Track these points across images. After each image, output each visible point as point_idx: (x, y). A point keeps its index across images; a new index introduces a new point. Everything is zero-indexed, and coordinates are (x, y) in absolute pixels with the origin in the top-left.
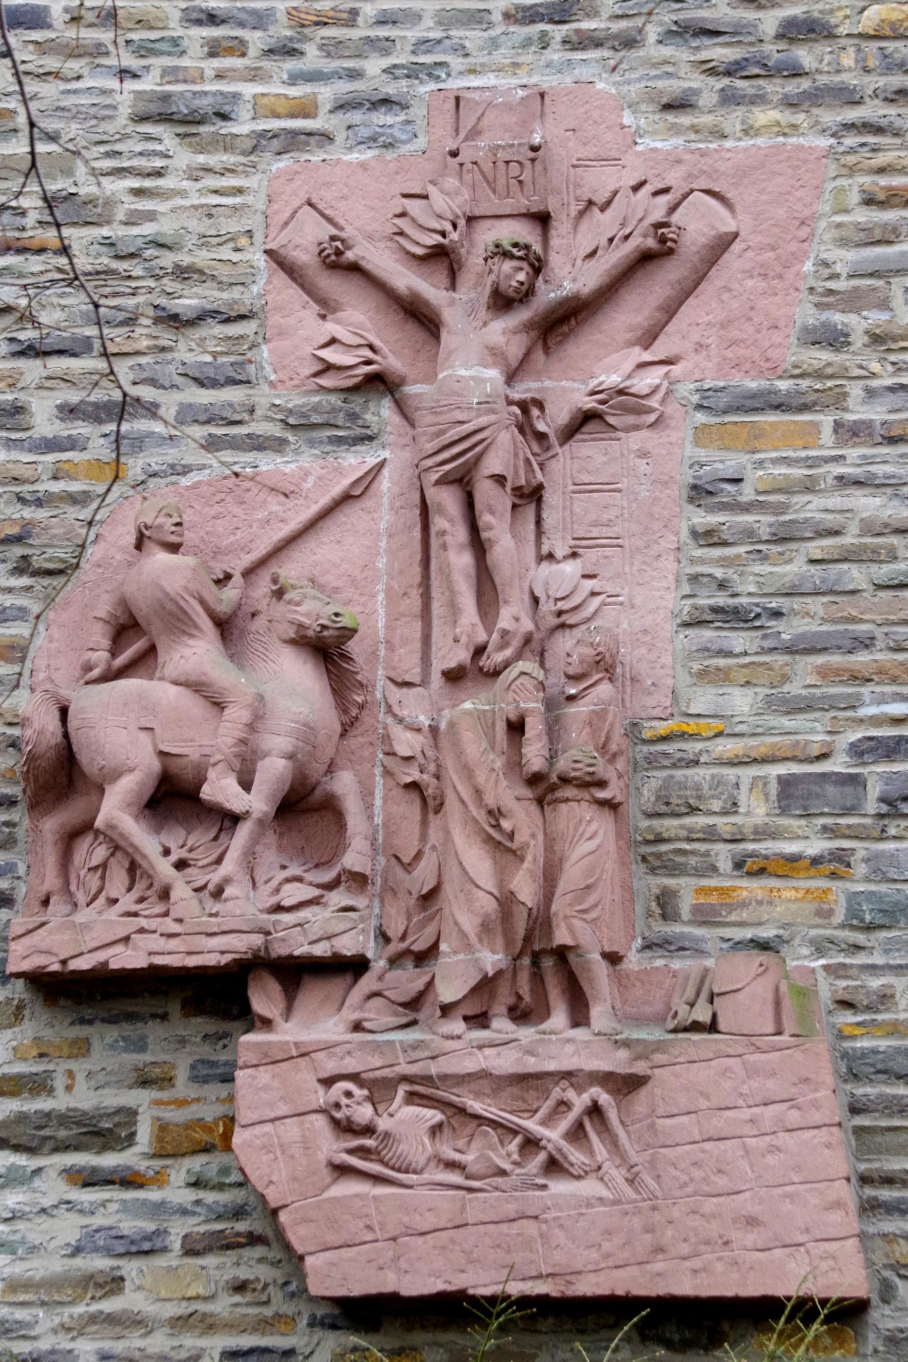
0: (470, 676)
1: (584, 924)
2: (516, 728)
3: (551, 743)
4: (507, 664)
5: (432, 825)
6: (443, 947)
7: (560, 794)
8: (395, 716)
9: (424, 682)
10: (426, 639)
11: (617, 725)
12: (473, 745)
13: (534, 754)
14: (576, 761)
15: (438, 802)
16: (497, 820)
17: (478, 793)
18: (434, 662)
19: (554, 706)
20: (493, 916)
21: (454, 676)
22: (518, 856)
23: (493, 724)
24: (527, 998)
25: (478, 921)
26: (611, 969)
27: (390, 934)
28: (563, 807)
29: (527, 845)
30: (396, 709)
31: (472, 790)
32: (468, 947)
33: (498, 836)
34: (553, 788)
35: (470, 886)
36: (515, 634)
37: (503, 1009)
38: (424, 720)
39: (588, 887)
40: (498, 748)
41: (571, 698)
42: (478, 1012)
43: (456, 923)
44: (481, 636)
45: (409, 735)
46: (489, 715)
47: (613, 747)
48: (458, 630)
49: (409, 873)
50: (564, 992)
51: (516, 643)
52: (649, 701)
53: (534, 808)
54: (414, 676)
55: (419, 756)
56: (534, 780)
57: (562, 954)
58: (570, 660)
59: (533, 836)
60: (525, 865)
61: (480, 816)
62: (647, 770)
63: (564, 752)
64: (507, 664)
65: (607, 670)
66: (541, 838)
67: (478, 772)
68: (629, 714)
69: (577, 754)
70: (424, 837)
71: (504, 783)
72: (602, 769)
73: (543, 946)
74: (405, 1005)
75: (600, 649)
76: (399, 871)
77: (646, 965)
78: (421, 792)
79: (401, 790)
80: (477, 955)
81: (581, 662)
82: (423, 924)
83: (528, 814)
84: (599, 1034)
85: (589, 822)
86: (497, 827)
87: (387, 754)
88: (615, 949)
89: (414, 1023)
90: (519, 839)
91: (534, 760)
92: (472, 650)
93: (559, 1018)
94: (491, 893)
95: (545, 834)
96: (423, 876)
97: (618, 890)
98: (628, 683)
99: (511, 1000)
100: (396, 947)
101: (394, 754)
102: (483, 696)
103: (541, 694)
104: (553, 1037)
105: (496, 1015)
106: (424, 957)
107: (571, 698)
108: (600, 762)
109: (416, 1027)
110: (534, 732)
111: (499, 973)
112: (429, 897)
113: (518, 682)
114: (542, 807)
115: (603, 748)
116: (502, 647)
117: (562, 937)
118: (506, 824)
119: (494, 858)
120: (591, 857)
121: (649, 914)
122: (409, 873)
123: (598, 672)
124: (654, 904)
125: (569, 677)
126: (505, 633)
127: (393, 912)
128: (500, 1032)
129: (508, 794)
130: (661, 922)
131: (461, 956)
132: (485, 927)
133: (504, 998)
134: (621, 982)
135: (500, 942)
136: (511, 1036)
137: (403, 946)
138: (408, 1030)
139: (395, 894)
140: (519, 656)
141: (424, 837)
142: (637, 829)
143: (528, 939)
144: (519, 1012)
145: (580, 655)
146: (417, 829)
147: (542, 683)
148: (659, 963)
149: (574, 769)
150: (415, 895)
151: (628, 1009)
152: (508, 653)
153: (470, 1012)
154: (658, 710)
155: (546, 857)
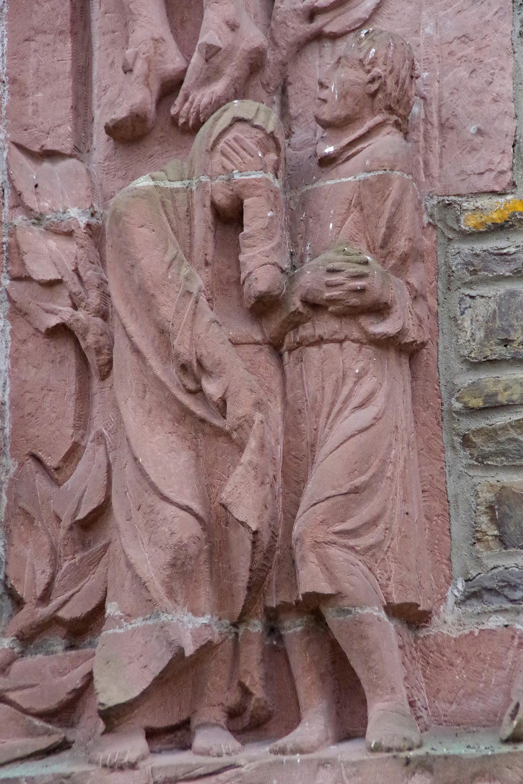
0: (157, 133)
1: (352, 557)
2: (229, 218)
3: (295, 244)
4: (217, 105)
5: (97, 399)
6: (112, 609)
7: (306, 331)
8: (28, 211)
9: (80, 150)
10: (82, 74)
11: (408, 207)
12: (151, 250)
13: (260, 263)
14: (332, 271)
15: (104, 358)
16: (198, 381)
17: (163, 334)
18: (97, 113)
19: (299, 178)
20: (193, 549)
21: (129, 134)
22: (233, 440)
23: (189, 213)
24: (258, 692)
25: (166, 557)
26: (408, 636)
27: (21, 591)
28: (314, 353)
29: (250, 421)
30: (30, 199)
31: (153, 331)
32: (149, 606)
33: (199, 410)
34: (295, 322)
35: (152, 499)
36: (230, 53)
37: (218, 715)
38: (78, 216)
39: (356, 490)
40: (198, 256)
41: (327, 162)
42: (174, 721)
43: (129, 566)
44: (173, 61)
45: (53, 244)
46: (181, 197)
47: (401, 245)
48: (129, 52)
49: (58, 484)
50: (322, 677)
51: (232, 70)
52: (473, 163)
53: (264, 358)
54: (61, 139)
55: (70, 279)
56: (263, 307)
57: (313, 608)
58: (324, 94)
59: (258, 405)
60: (247, 457)
61: (168, 375)
62: (469, 284)
63: (314, 256)
64: (217, 105)
65: (390, 109)
66: (276, 409)
67: (161, 298)
68: (438, 187)
69: (338, 255)
70: (83, 421)
71: (208, 315)
72: (378, 282)
73: (285, 597)
74: (47, 716)
75: (377, 70)
76: (41, 483)
77: (472, 627)
78: (77, 342)
79: (41, 340)
80: (164, 618)
81: (343, 96)
82: (80, 573)
83: (252, 369)
84: (377, 749)
85: (359, 377)
86: (198, 392)
87: (16, 279)
88: (411, 598)
89: (63, 746)
90: (236, 410)
91: (259, 273)
92: (156, 87)
93: (313, 726)
94: (187, 509)
95: (285, 403)
96: (82, 488)
97: (416, 496)
98: (435, 132)
99: (233, 698)
100: (33, 613)
101: (28, 279)
102: (173, 165)
103: (273, 156)
104: (298, 758)
105: (204, 725)
106: (82, 630)
107: (327, 162)
108: (375, 267)
109: (66, 754)
110: (260, 224)
111: (207, 649)
112: (92, 523)
113: (229, 136)
114: (280, 356)
115: (383, 247)
116: (207, 80)
117: (312, 579)
118: (212, 388)
119: (195, 448)
120: (364, 436)
121: (478, 539)
122: (58, 484)
123: (373, 112)
124: (484, 519)
125: (327, 125)
126: (212, 52)
127: (28, 552)
128: (206, 753)
129: (217, 336)
130: (497, 549)
131: (138, 623)
132: (180, 570)
133: (219, 695)
134: (428, 658)
135: (205, 594)
136: (225, 760)
137: (44, 611)
138: (52, 759)
139: (31, 520)
140: (239, 92)
141: (83, 421)
142: (453, 390)
143: (256, 587)
144: (246, 719)
145: (342, 83)
146: (70, 408)
147: (272, 136)
148: (495, 622)
149: (330, 286)
150: (66, 522)
151: (442, 706)
152: (219, 87)
153: (158, 722)
154: (488, 177)
155: (287, 443)
